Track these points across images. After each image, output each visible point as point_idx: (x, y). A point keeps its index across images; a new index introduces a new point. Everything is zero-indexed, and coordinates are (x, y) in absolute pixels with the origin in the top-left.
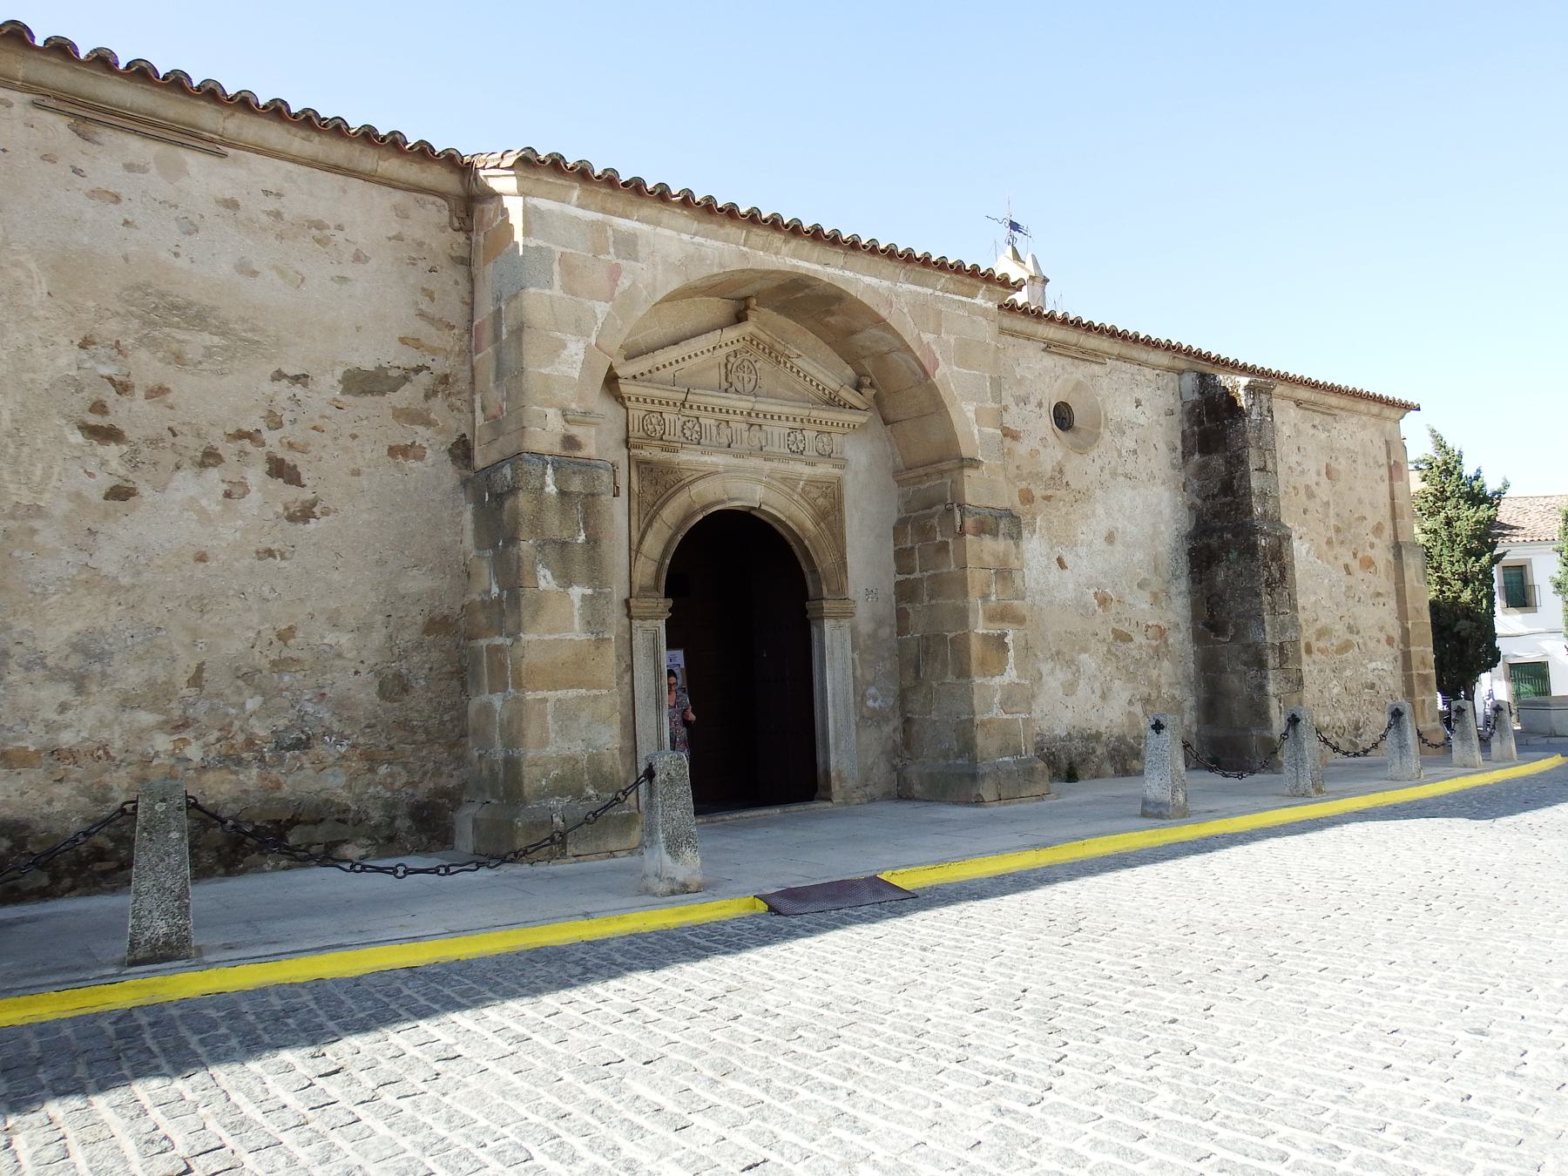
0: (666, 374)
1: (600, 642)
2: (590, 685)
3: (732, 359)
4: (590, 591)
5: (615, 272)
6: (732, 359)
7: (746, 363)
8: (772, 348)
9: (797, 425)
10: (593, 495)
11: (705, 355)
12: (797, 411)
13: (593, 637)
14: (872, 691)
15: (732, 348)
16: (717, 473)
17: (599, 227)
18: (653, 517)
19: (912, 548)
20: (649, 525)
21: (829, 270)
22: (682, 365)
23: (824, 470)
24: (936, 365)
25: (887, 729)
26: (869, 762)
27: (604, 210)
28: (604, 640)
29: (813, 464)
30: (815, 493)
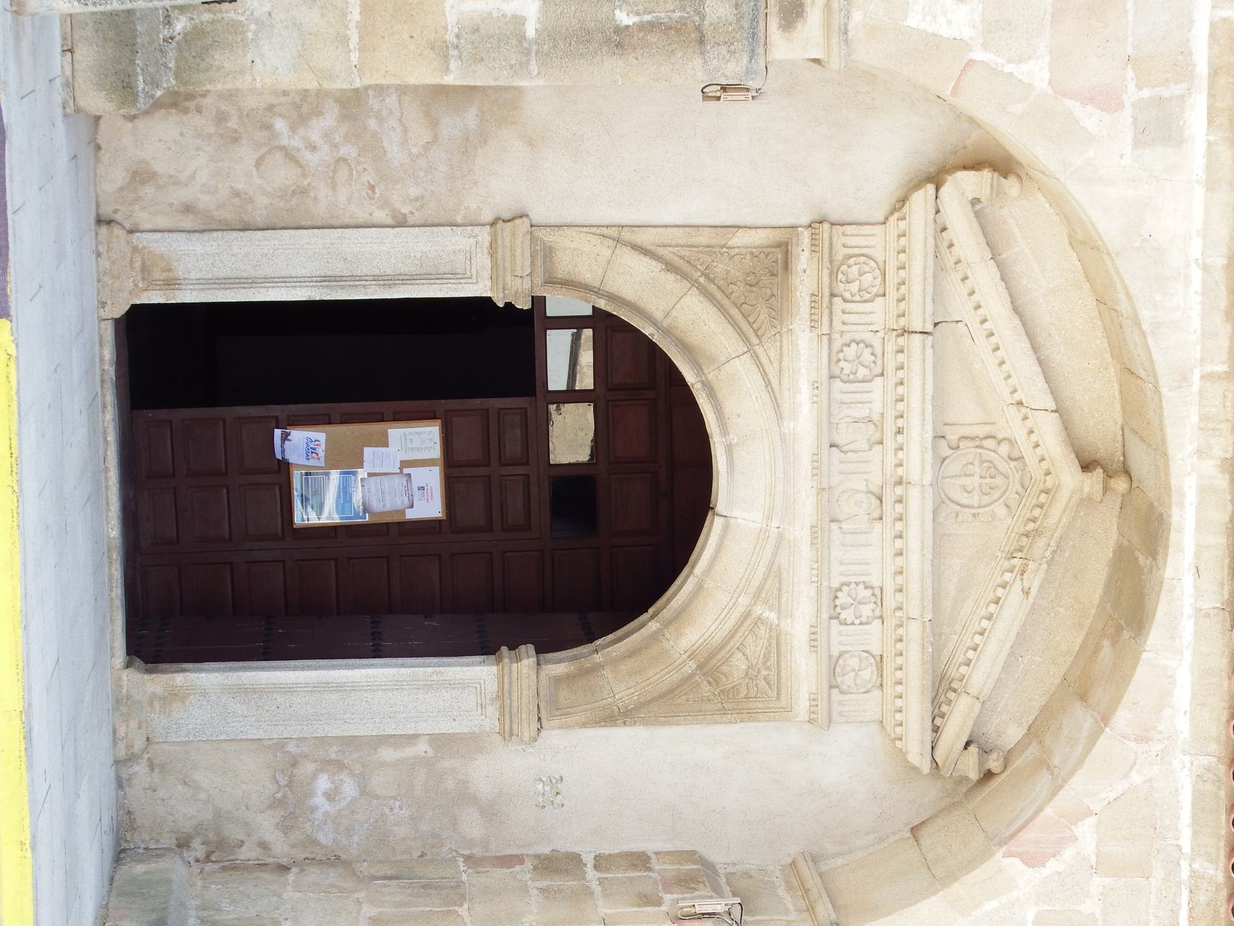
0: (959, 307)
1: (442, 51)
2: (365, 31)
3: (1004, 449)
4: (531, 31)
5: (1107, 100)
6: (1004, 449)
7: (999, 480)
8: (1037, 533)
9: (890, 601)
10: (701, 41)
11: (1002, 385)
12: (914, 588)
13: (450, 37)
14: (349, 789)
15: (1025, 448)
16: (779, 417)
17: (1182, 69)
18: (684, 276)
19: (650, 869)
20: (670, 267)
21: (1188, 580)
22: (980, 335)
23: (804, 671)
24: (1032, 861)
25: (267, 826)
26: (199, 777)
27: (1214, 73)
28: (446, 57)
29: (813, 643)
30: (756, 648)
